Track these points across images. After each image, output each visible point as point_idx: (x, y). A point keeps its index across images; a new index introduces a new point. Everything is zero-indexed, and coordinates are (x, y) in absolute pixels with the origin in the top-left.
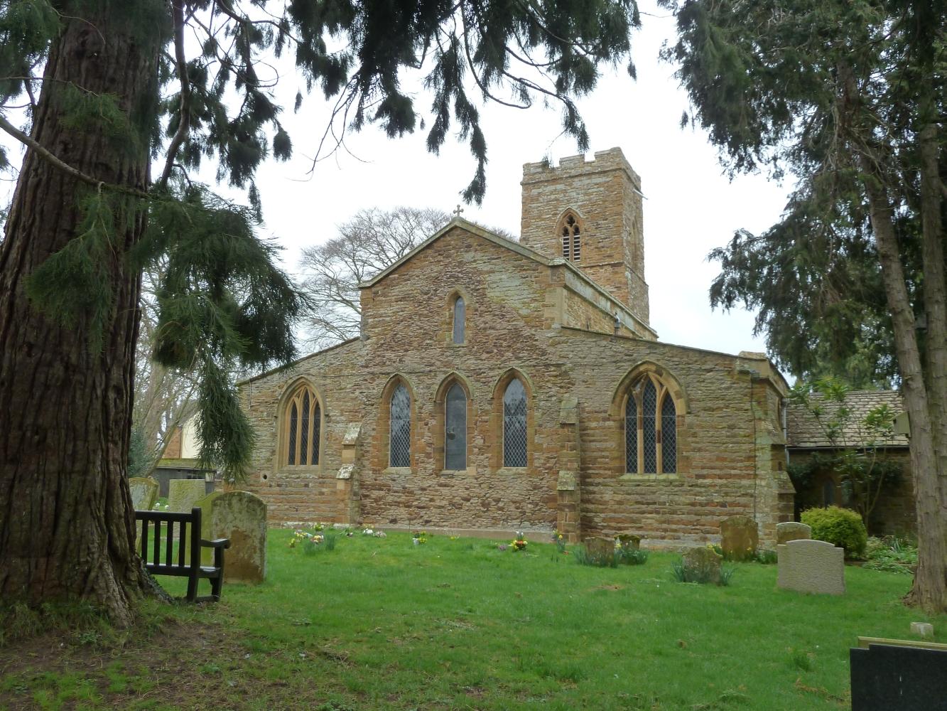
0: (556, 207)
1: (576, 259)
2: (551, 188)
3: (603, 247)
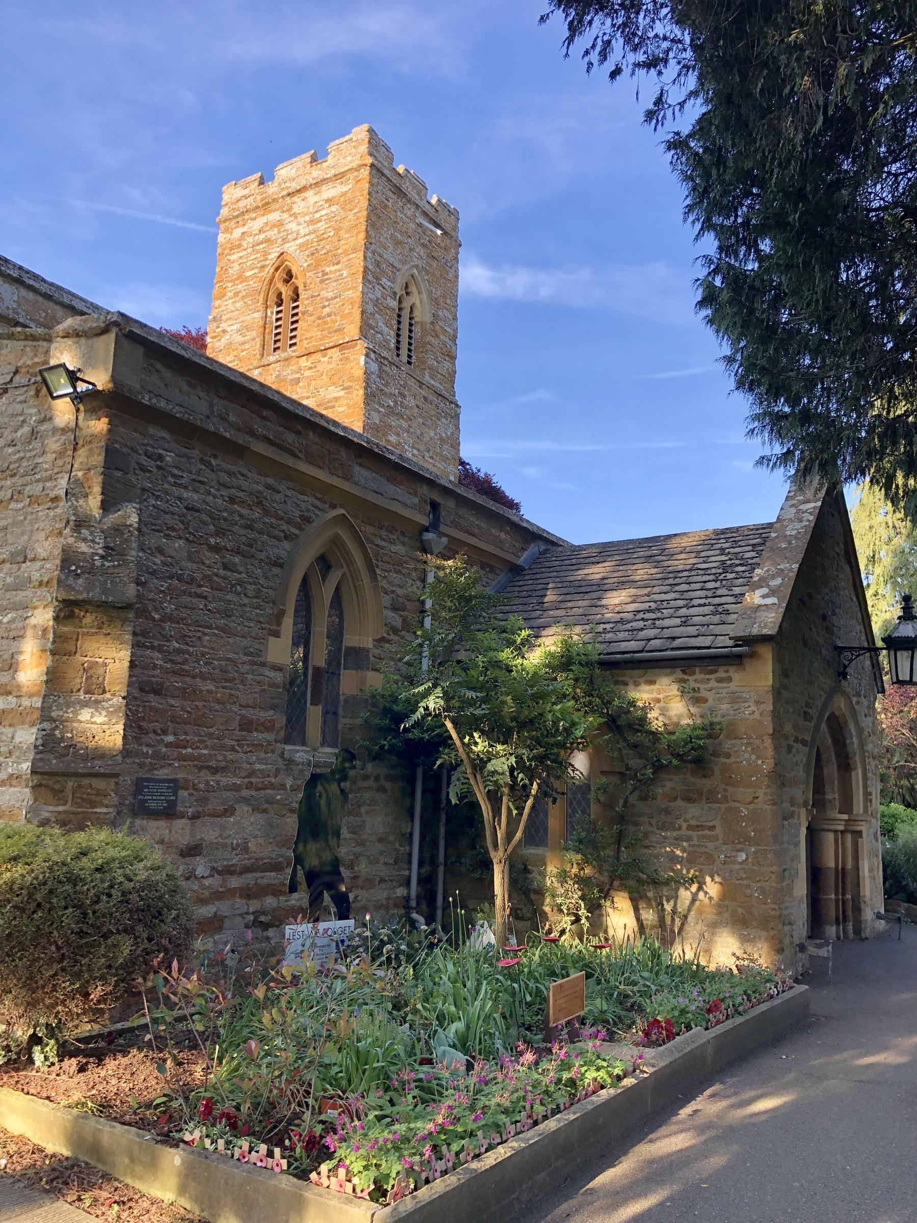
0: (265, 254)
1: (291, 345)
2: (260, 222)
3: (329, 315)
